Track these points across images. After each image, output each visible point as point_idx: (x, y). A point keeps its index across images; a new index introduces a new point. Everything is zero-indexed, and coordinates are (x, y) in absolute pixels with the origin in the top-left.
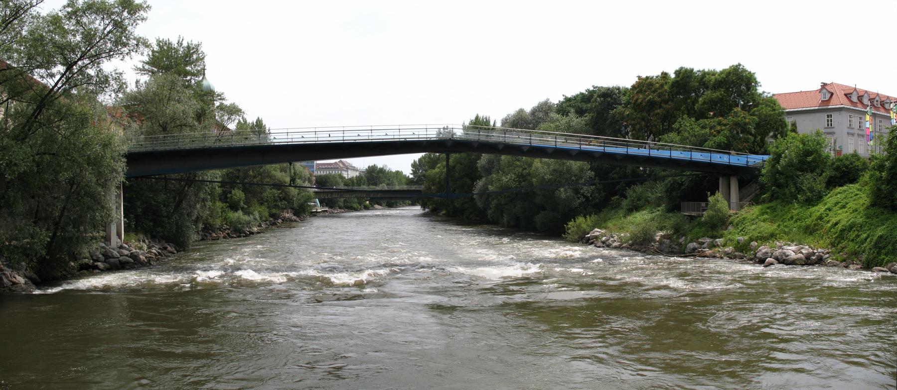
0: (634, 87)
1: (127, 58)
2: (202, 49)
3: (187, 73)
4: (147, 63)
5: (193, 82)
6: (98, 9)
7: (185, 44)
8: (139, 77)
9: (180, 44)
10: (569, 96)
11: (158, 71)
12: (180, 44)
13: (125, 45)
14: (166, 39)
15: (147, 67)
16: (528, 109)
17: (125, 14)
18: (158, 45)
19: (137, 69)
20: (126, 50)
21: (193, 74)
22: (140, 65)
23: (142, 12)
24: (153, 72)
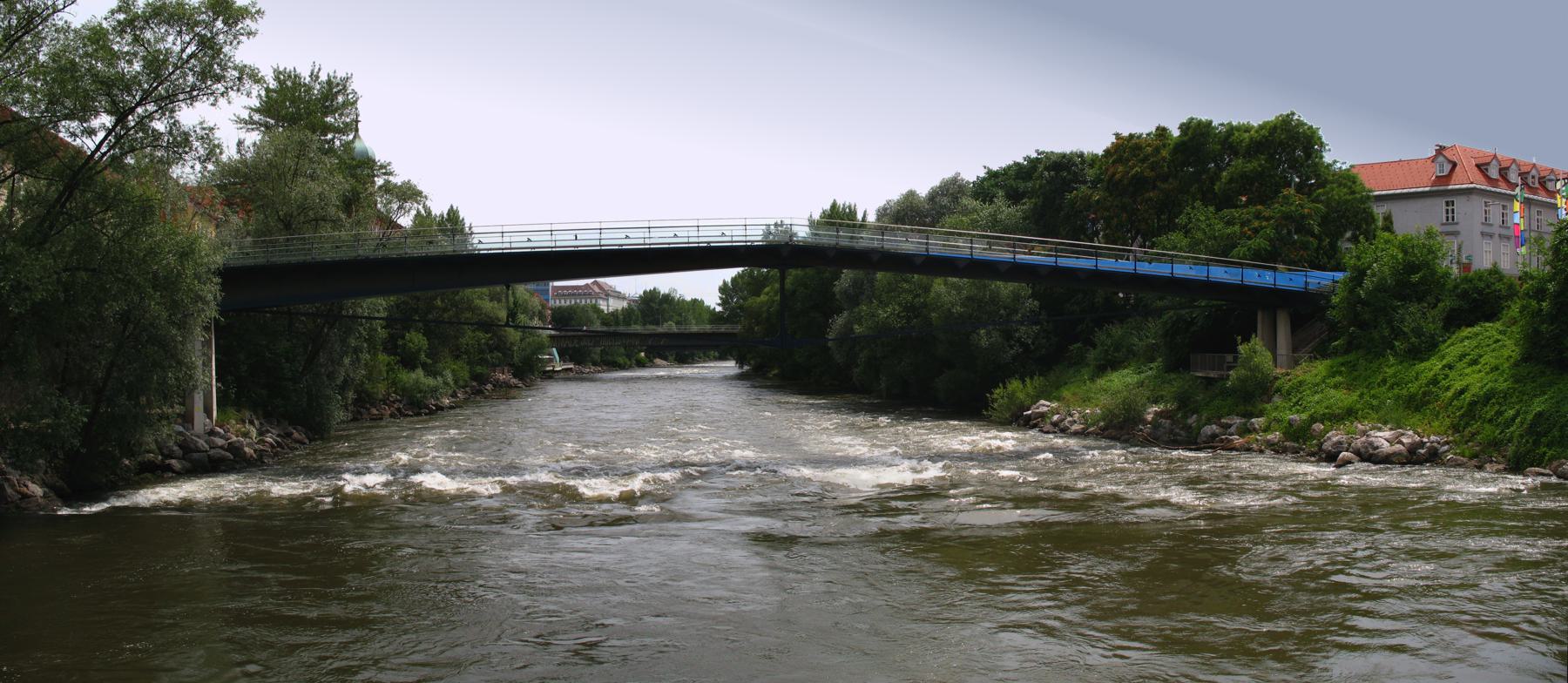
0: (1107, 151)
1: (222, 101)
2: (354, 85)
3: (328, 128)
4: (257, 110)
5: (337, 143)
6: (171, 16)
7: (323, 77)
8: (243, 135)
9: (314, 76)
10: (995, 168)
11: (277, 125)
12: (314, 76)
13: (218, 79)
14: (290, 68)
15: (256, 117)
16: (923, 191)
17: (219, 24)
18: (277, 78)
19: (240, 121)
20: (220, 87)
21: (338, 130)
22: (245, 115)
23: (248, 21)
24: (267, 126)
